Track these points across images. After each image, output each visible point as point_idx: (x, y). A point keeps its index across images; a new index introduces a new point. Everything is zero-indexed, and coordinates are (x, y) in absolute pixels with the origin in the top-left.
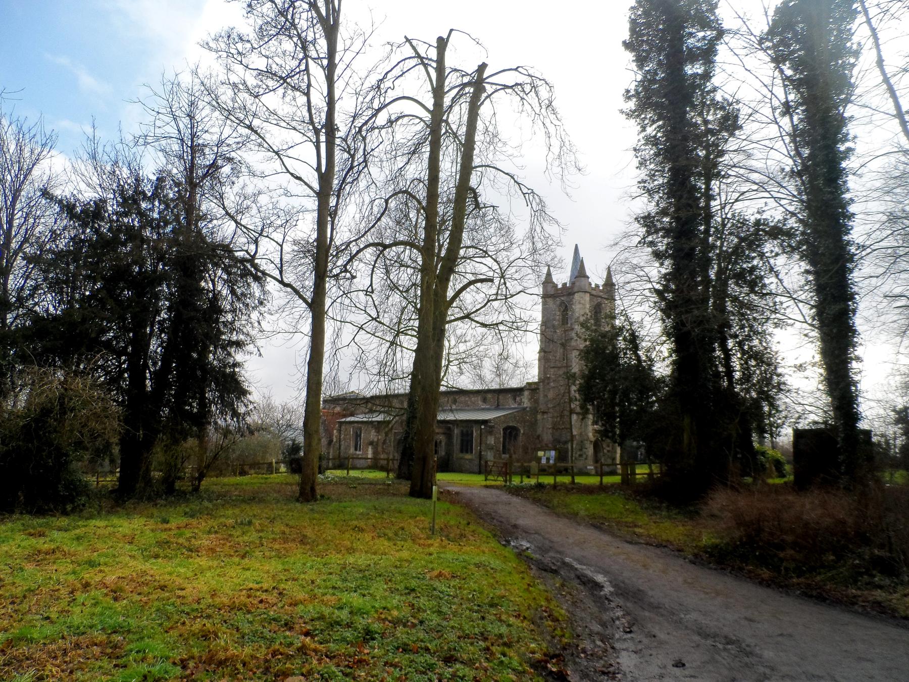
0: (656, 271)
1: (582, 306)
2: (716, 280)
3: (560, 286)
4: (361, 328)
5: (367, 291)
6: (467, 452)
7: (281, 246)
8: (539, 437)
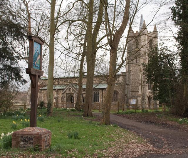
0: (176, 29)
1: (144, 41)
2: (182, 71)
3: (135, 32)
4: (62, 53)
5: (65, 38)
6: (97, 101)
7: (39, 24)
8: (126, 95)
